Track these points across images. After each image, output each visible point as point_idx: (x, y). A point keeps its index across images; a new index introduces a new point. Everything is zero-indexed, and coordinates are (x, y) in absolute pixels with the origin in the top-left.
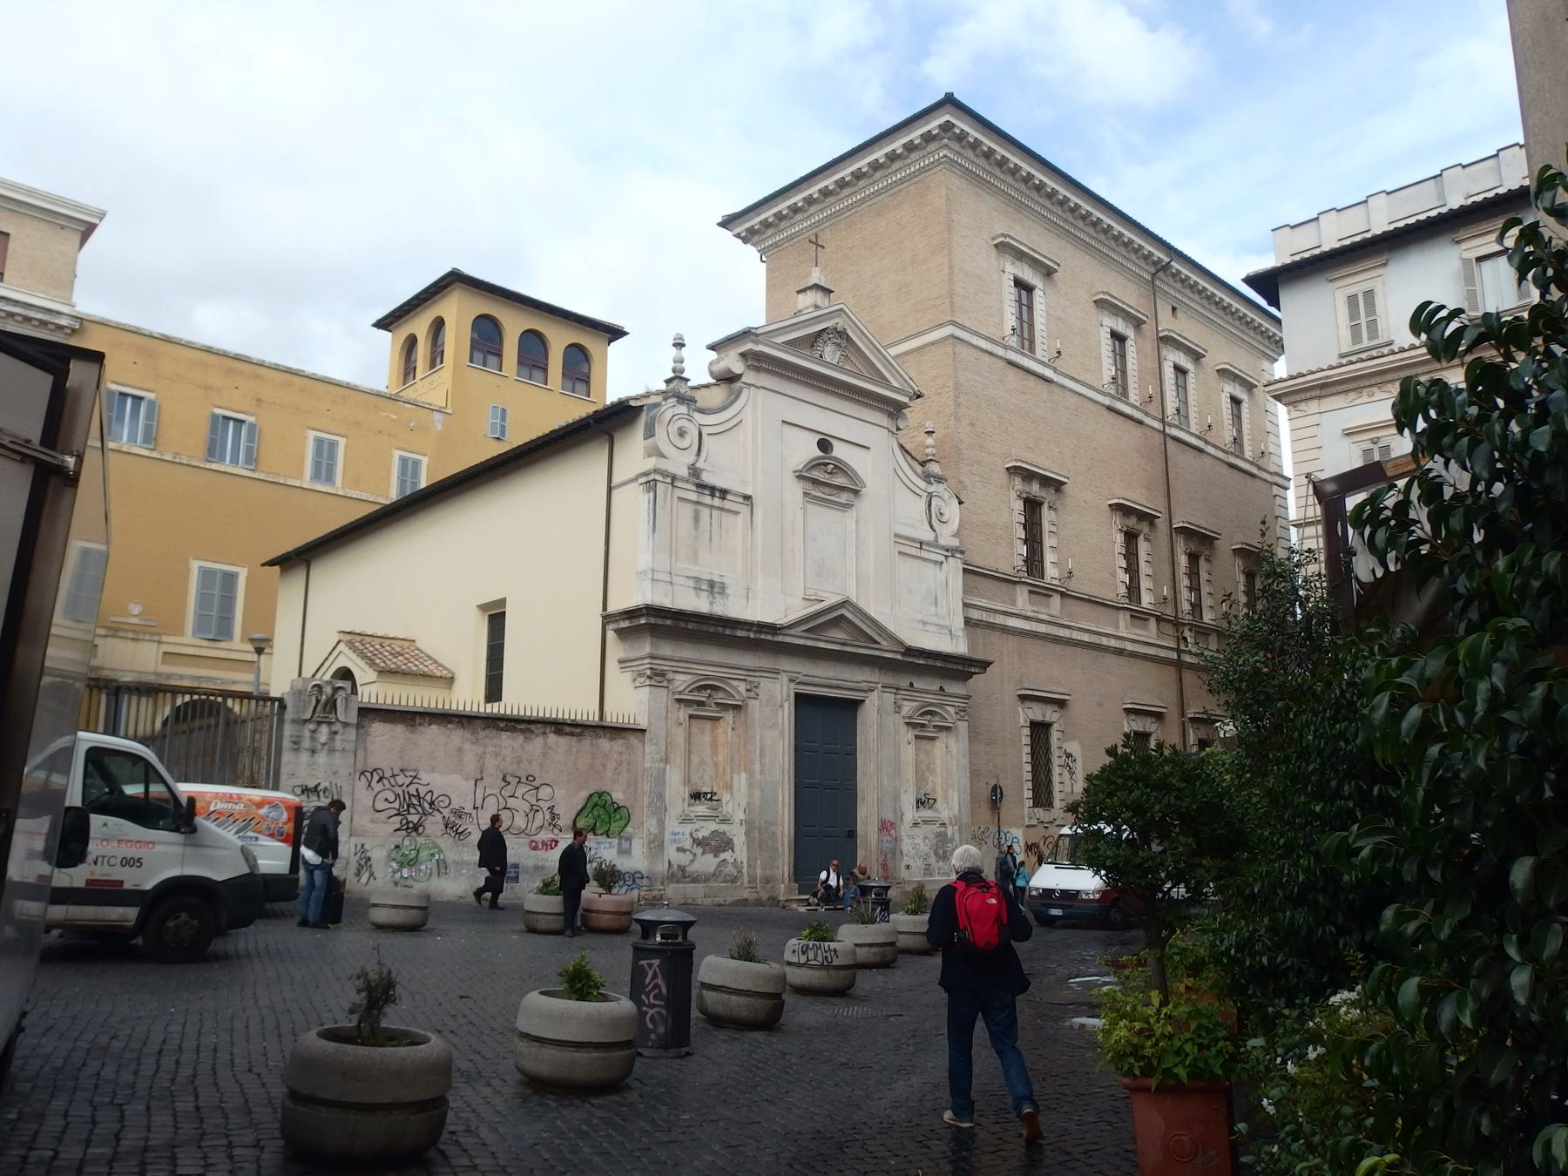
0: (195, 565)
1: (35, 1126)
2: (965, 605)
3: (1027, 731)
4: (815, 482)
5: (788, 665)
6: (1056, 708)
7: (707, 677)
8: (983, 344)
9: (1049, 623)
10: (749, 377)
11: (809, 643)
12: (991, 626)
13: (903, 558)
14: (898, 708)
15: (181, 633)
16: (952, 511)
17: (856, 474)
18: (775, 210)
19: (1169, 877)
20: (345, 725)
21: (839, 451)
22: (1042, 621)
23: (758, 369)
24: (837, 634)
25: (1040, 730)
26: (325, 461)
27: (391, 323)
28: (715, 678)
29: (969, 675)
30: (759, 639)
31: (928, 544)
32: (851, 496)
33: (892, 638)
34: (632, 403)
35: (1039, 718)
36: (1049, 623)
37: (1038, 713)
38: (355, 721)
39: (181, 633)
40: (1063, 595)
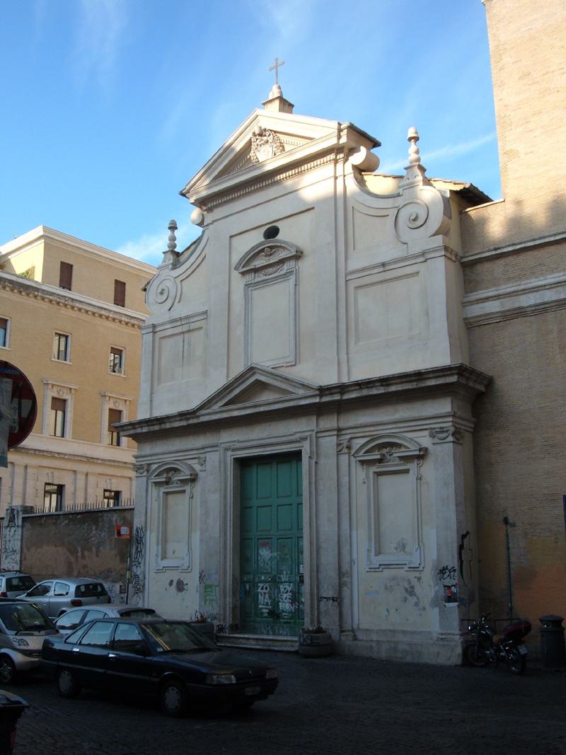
4: (256, 270)
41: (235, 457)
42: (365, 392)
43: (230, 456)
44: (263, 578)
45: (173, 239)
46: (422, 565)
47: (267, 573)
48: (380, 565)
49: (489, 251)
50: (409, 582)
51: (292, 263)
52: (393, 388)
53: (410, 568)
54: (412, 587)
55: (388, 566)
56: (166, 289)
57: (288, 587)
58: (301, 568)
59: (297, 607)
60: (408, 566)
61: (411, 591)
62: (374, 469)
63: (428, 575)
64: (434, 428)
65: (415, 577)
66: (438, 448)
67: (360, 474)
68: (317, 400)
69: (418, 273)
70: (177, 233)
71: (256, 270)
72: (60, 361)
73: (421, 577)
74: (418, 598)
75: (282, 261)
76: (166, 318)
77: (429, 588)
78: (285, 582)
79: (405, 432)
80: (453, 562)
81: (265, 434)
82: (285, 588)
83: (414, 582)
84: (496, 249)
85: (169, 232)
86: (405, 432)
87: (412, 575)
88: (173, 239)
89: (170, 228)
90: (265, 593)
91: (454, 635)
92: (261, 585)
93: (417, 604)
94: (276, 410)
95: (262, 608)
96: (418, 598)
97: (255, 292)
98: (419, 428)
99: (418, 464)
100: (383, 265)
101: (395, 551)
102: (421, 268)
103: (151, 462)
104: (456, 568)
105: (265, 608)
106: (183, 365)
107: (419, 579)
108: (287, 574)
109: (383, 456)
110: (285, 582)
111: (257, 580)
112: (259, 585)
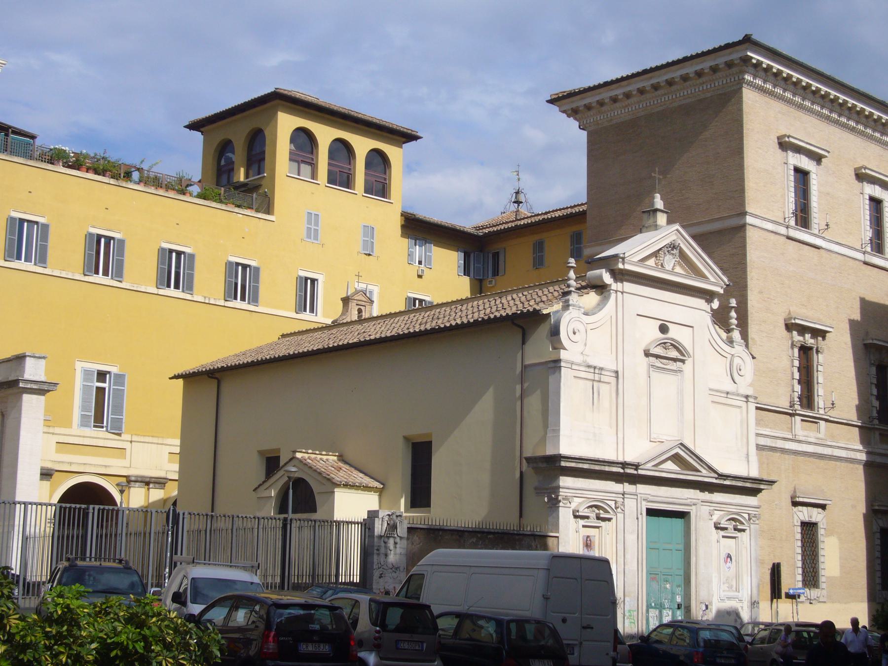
0: (79, 366)
3: (799, 529)
6: (820, 510)
8: (770, 226)
9: (816, 444)
12: (773, 449)
13: (714, 405)
15: (69, 425)
16: (748, 367)
18: (598, 98)
19: (20, 653)
20: (401, 538)
21: (675, 333)
22: (810, 443)
24: (690, 472)
25: (809, 529)
27: (203, 126)
29: (759, 491)
30: (627, 474)
31: (733, 394)
32: (681, 364)
35: (807, 519)
36: (816, 444)
37: (804, 514)
38: (406, 535)
39: (69, 425)
40: (826, 420)
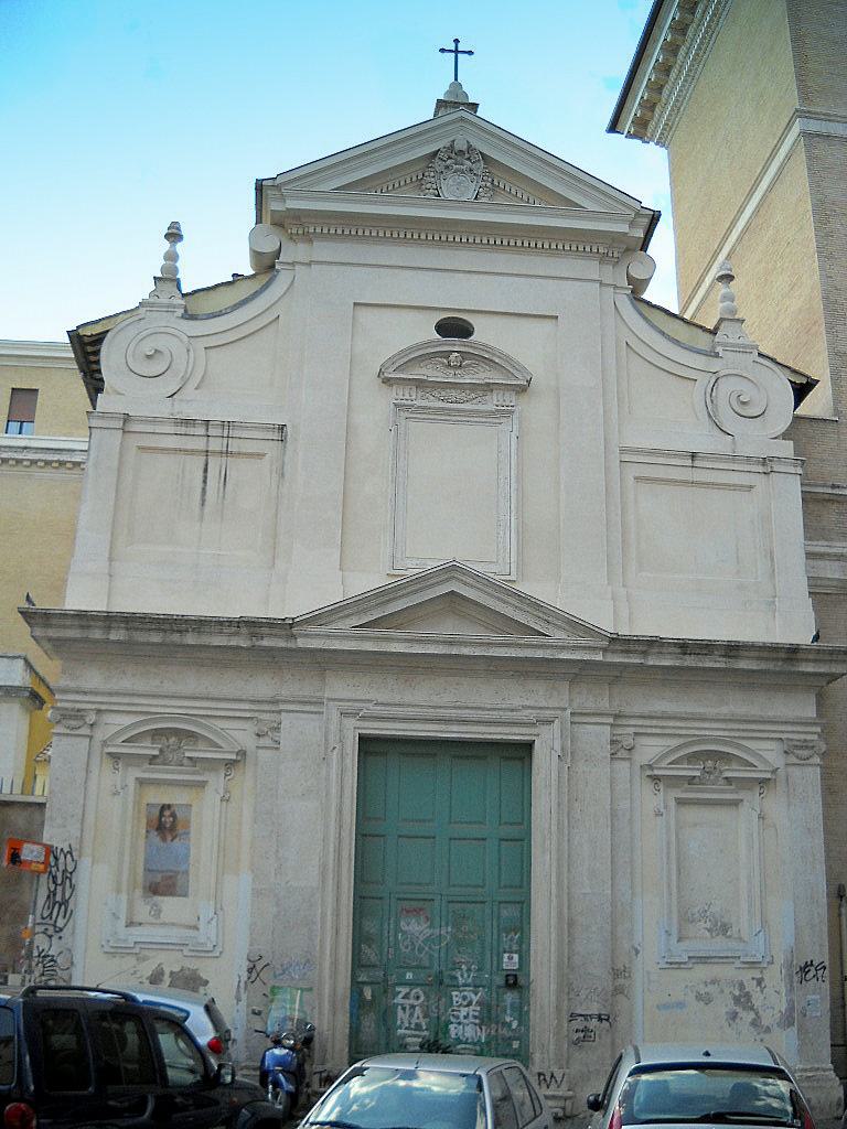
1: (17, 1124)
2: (810, 555)
4: (420, 384)
5: (341, 688)
7: (702, 740)
10: (293, 252)
11: (369, 646)
14: (619, 750)
17: (508, 359)
23: (308, 238)
26: (373, 603)
28: (716, 740)
30: (262, 645)
33: (575, 625)
34: (88, 332)
41: (364, 732)
42: (689, 661)
43: (352, 731)
44: (409, 976)
45: (171, 257)
46: (219, 949)
47: (418, 967)
48: (689, 957)
49: (824, 486)
50: (742, 986)
51: (510, 398)
52: (743, 665)
53: (744, 963)
54: (748, 995)
55: (704, 960)
56: (167, 353)
57: (473, 996)
58: (505, 960)
59: (493, 1032)
60: (734, 966)
61: (743, 1000)
62: (136, 773)
63: (776, 977)
64: (792, 740)
65: (753, 979)
66: (796, 772)
67: (651, 800)
68: (599, 657)
69: (751, 487)
70: (179, 247)
71: (420, 384)
72: (24, 436)
73: (762, 979)
74: (757, 1014)
75: (489, 387)
76: (164, 410)
77: (774, 998)
78: (465, 985)
79: (744, 738)
80: (820, 953)
81: (446, 699)
82: (464, 998)
83: (751, 987)
84: (833, 487)
85: (166, 245)
86: (739, 737)
87: (747, 976)
88: (171, 257)
89: (167, 236)
90: (413, 1007)
91: (824, 1070)
92: (404, 990)
93: (754, 1024)
94: (350, 652)
95: (405, 1036)
96: (757, 1014)
97: (412, 424)
98: (750, 735)
99: (226, 775)
100: (693, 456)
101: (708, 934)
102: (759, 481)
103: (103, 707)
104: (827, 964)
105: (415, 1036)
106: (201, 518)
107: (759, 982)
108: (469, 970)
109: (706, 775)
110: (465, 985)
111: (393, 979)
112: (398, 989)
